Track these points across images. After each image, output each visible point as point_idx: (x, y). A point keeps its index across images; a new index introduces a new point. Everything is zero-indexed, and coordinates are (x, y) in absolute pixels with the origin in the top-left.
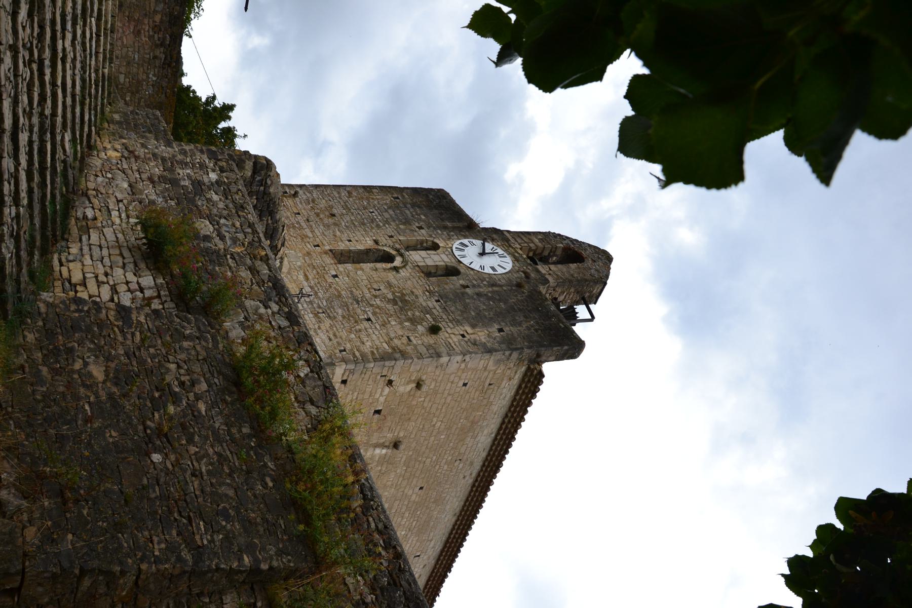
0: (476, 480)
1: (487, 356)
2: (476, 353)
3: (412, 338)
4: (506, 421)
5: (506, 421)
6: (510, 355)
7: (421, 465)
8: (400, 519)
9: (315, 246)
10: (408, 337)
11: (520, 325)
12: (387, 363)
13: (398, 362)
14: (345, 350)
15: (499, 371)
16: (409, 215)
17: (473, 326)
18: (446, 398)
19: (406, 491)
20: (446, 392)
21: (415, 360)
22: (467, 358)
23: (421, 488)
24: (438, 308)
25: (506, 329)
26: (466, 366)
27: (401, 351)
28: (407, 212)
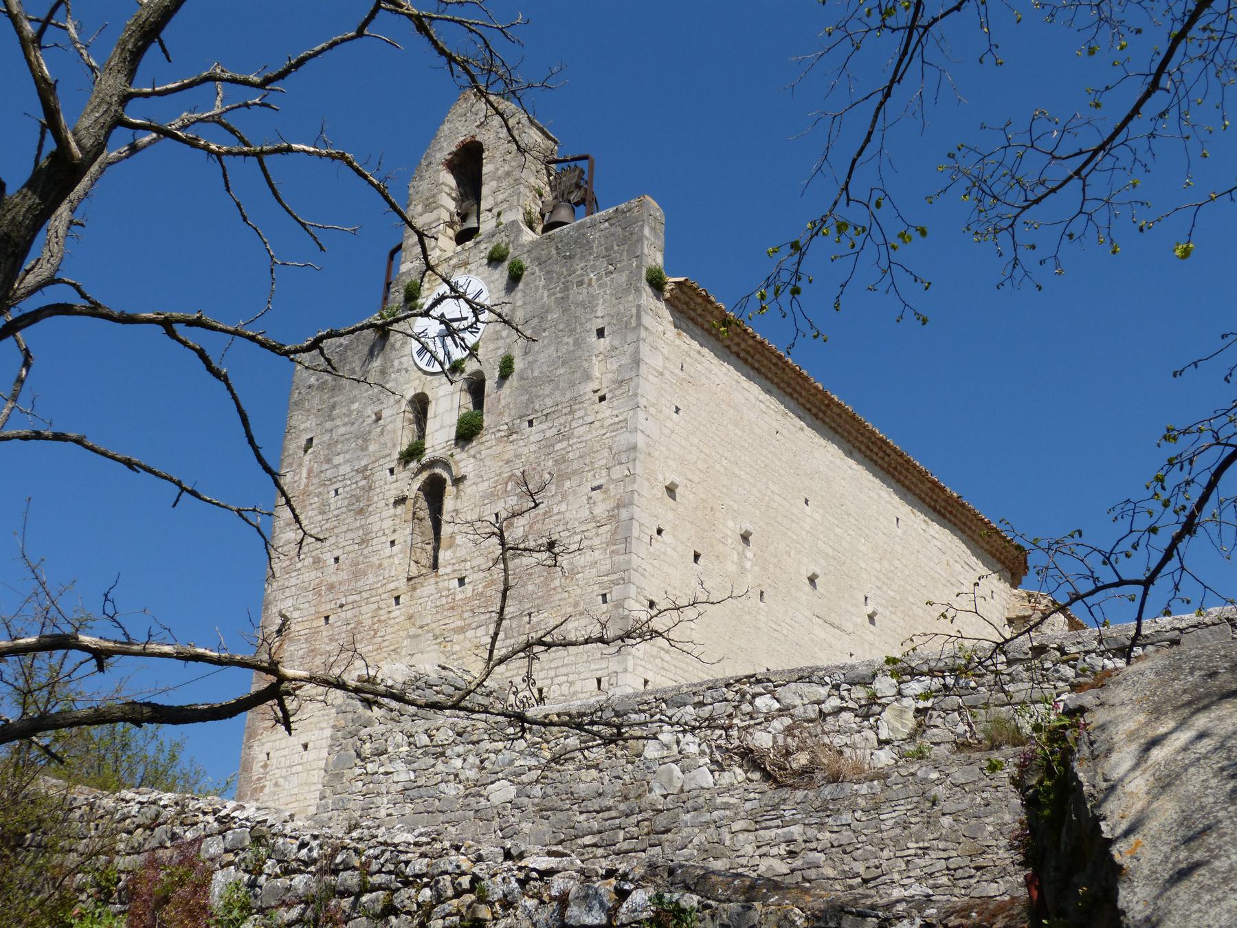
0: (810, 410)
1: (643, 369)
2: (637, 386)
3: (596, 484)
4: (735, 348)
5: (735, 348)
6: (646, 329)
7: (776, 497)
8: (843, 542)
9: (397, 603)
10: (593, 489)
11: (593, 297)
12: (635, 533)
13: (636, 516)
14: (604, 596)
15: (665, 351)
16: (348, 429)
17: (588, 377)
18: (692, 445)
19: (807, 528)
20: (683, 442)
21: (635, 487)
22: (642, 402)
23: (806, 502)
24: (544, 426)
25: (599, 323)
26: (653, 405)
27: (618, 507)
28: (342, 430)
